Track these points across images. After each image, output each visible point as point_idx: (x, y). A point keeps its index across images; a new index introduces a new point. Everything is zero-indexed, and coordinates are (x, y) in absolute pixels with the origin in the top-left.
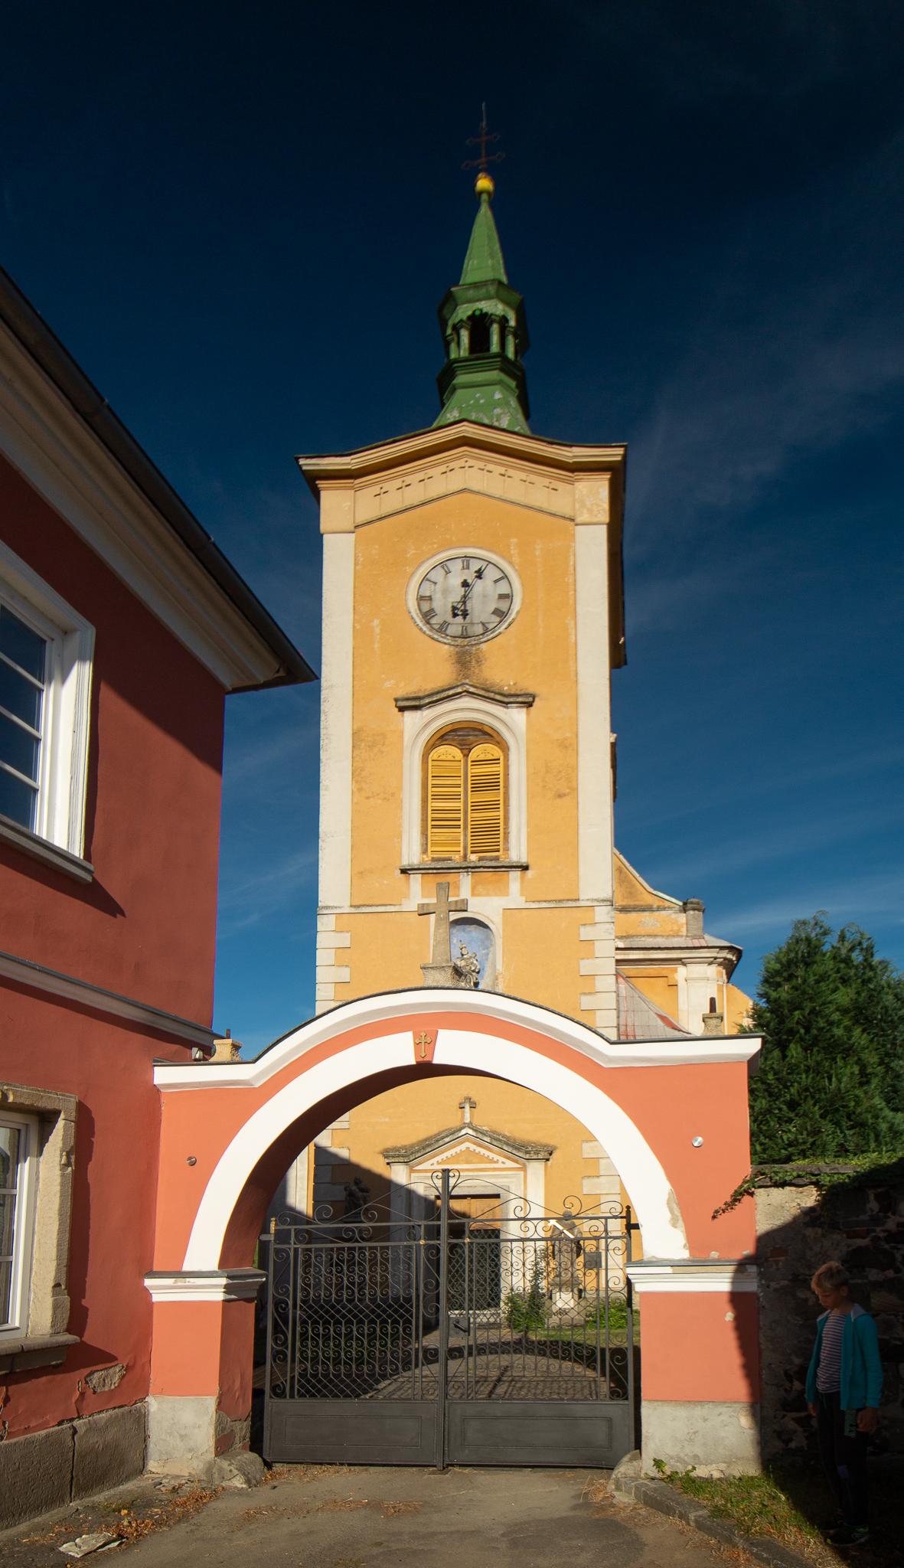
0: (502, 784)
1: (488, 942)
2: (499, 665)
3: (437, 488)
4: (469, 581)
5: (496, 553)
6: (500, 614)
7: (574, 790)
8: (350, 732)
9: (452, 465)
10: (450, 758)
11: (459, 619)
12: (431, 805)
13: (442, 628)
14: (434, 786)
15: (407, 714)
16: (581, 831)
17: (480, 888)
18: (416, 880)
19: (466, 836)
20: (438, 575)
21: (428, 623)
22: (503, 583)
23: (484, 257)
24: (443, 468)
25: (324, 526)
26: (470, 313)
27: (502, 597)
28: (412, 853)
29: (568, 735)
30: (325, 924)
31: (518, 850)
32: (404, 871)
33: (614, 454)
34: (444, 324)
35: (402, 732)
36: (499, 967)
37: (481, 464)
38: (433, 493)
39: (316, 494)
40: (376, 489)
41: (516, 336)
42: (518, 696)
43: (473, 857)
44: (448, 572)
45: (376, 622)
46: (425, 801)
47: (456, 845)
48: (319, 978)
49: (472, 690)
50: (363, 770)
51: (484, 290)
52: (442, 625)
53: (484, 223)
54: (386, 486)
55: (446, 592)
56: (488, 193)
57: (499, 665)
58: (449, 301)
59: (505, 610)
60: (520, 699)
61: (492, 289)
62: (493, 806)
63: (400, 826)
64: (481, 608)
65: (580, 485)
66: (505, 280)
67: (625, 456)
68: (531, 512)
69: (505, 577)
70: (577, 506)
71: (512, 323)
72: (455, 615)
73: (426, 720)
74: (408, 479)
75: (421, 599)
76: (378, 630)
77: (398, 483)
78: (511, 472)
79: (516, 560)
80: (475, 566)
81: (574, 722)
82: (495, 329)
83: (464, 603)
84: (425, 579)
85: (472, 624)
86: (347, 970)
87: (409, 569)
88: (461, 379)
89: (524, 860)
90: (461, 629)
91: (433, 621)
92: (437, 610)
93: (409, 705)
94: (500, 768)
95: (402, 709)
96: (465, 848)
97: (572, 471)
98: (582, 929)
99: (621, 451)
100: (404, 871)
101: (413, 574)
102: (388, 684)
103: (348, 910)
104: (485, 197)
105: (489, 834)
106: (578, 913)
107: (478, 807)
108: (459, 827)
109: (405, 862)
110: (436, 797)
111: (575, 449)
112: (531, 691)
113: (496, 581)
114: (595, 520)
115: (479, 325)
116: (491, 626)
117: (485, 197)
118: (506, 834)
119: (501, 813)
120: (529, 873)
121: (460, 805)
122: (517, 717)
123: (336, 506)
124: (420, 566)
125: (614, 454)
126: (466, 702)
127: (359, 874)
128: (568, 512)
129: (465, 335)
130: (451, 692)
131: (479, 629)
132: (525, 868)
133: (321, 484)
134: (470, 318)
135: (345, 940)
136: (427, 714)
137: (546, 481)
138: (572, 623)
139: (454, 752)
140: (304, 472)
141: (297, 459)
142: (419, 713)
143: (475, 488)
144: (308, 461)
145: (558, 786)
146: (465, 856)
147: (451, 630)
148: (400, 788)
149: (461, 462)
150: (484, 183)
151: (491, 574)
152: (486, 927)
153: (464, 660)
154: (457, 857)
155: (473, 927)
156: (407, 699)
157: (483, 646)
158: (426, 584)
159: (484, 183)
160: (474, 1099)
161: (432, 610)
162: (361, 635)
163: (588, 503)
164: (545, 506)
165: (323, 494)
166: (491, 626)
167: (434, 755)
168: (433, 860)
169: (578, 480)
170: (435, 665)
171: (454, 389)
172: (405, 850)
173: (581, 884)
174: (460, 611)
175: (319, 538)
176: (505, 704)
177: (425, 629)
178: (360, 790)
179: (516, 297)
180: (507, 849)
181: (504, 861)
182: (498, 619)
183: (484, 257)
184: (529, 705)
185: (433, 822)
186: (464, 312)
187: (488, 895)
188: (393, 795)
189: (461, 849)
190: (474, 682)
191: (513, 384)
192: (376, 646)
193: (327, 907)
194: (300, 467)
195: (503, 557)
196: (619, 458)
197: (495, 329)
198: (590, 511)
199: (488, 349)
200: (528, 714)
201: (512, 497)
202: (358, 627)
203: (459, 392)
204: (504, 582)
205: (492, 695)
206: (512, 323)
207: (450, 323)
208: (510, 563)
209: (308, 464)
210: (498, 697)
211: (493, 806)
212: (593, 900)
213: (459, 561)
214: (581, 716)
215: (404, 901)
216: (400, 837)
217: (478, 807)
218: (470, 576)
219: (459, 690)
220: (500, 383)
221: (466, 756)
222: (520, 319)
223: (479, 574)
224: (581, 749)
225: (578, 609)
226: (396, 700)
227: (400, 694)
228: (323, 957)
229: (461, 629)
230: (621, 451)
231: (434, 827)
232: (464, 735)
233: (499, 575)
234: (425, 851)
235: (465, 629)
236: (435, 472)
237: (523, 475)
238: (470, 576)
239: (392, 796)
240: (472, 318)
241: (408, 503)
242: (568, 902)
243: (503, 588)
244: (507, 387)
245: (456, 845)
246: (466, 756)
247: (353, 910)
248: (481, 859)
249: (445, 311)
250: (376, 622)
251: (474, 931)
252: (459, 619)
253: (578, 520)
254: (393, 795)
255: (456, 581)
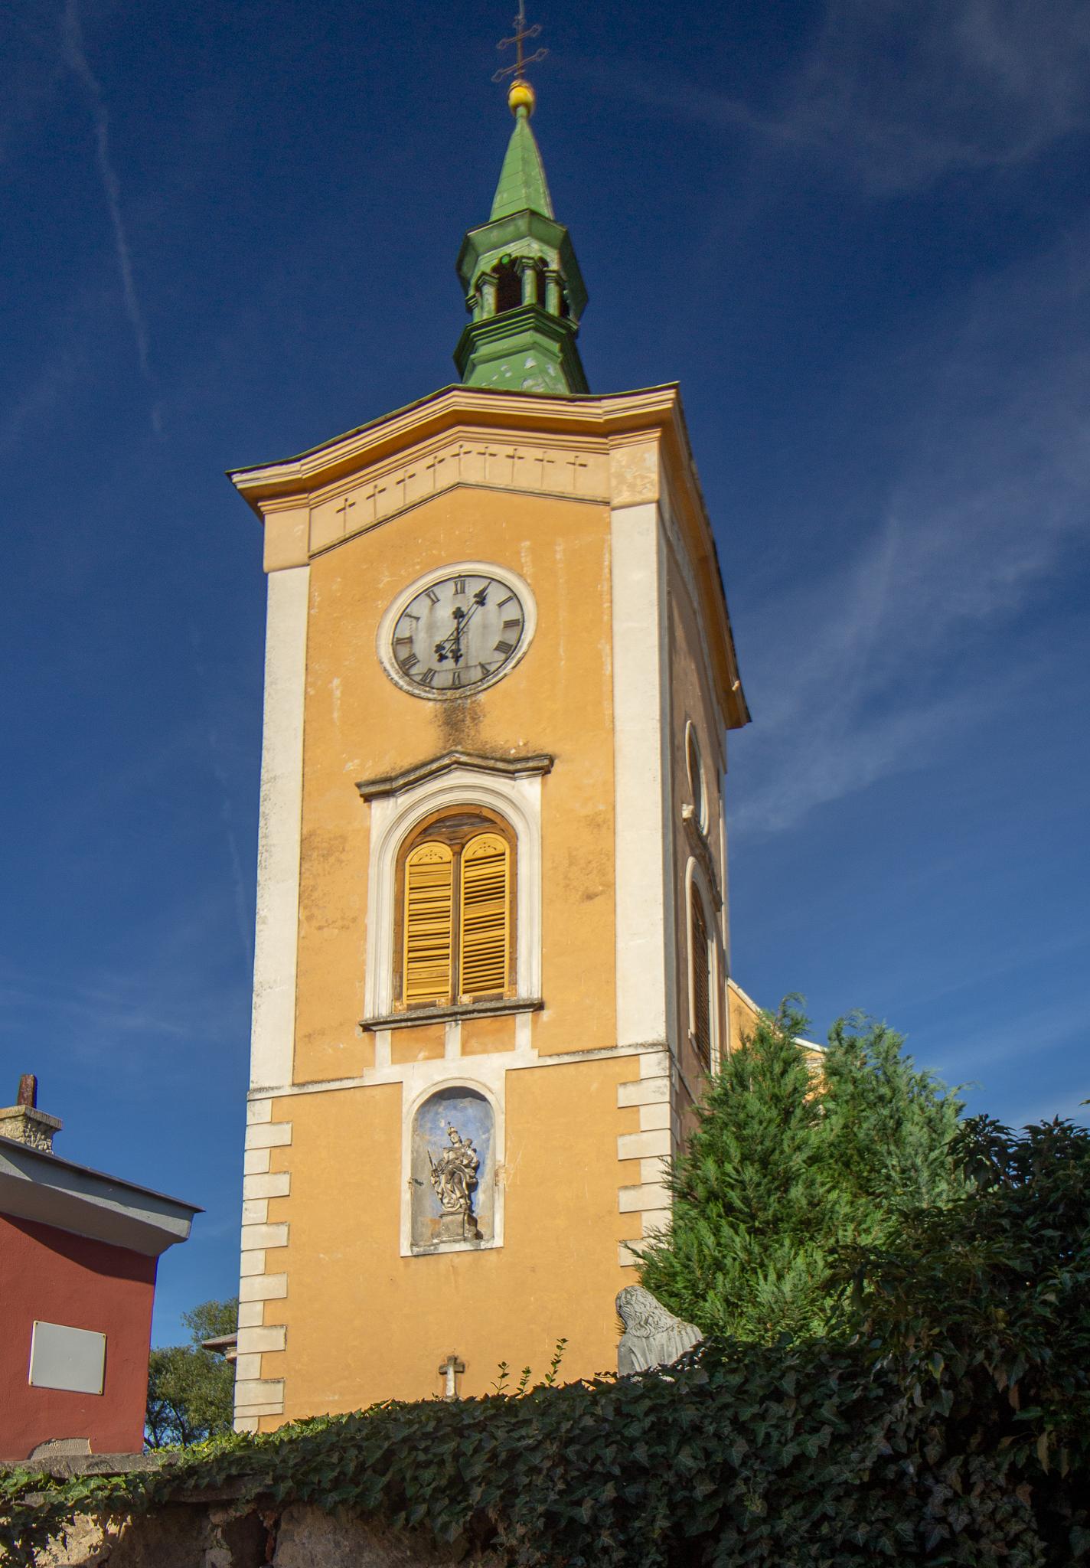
0: (507, 889)
1: (486, 1123)
2: (503, 722)
3: (419, 489)
4: (464, 609)
5: (500, 565)
6: (506, 648)
7: (610, 886)
8: (298, 837)
9: (441, 455)
10: (436, 859)
11: (449, 664)
12: (408, 928)
13: (426, 680)
14: (412, 902)
15: (375, 804)
16: (620, 945)
17: (474, 1043)
18: (384, 1040)
19: (456, 969)
20: (422, 608)
21: (407, 674)
22: (512, 606)
23: (522, 181)
24: (429, 460)
25: (267, 565)
26: (495, 262)
27: (509, 624)
28: (379, 1000)
29: (602, 807)
30: (258, 1113)
31: (528, 984)
32: (367, 1028)
33: (663, 400)
34: (465, 283)
35: (368, 831)
36: (500, 1157)
37: (481, 447)
38: (414, 497)
39: (261, 517)
40: (339, 503)
41: (560, 283)
42: (527, 759)
43: (465, 999)
44: (435, 601)
45: (336, 682)
46: (398, 924)
47: (436, 985)
48: (247, 1193)
49: (463, 759)
50: (314, 889)
51: (511, 229)
52: (425, 675)
53: (522, 141)
54: (352, 497)
55: (431, 627)
56: (526, 105)
57: (503, 722)
58: (467, 249)
59: (513, 642)
60: (531, 764)
61: (522, 224)
62: (496, 921)
63: (364, 963)
64: (479, 645)
65: (617, 454)
66: (547, 212)
67: (678, 401)
68: (548, 502)
69: (514, 597)
70: (614, 482)
71: (554, 266)
72: (442, 658)
73: (401, 810)
74: (381, 483)
75: (397, 642)
76: (338, 694)
77: (369, 489)
78: (522, 451)
79: (528, 570)
80: (474, 588)
81: (609, 789)
82: (529, 277)
83: (457, 640)
84: (405, 614)
85: (467, 667)
86: (286, 1178)
87: (380, 604)
88: (484, 350)
89: (536, 995)
90: (450, 674)
91: (413, 671)
92: (419, 656)
93: (378, 790)
94: (506, 867)
95: (368, 798)
96: (455, 986)
97: (606, 436)
98: (621, 1091)
99: (671, 394)
100: (367, 1028)
101: (386, 610)
102: (350, 766)
103: (288, 1091)
104: (522, 111)
105: (490, 963)
106: (615, 1067)
107: (473, 926)
108: (446, 957)
109: (368, 1015)
110: (415, 918)
111: (605, 403)
112: (549, 750)
113: (500, 605)
114: (638, 498)
115: (508, 277)
116: (492, 668)
117: (522, 111)
118: (514, 960)
119: (506, 931)
120: (545, 1015)
121: (448, 925)
122: (529, 790)
123: (284, 531)
124: (396, 598)
125: (663, 400)
126: (458, 778)
127: (305, 1038)
128: (600, 493)
129: (490, 294)
130: (435, 766)
131: (477, 674)
132: (538, 1007)
133: (265, 506)
134: (495, 269)
135: (282, 1135)
136: (404, 800)
137: (570, 456)
138: (608, 647)
139: (444, 851)
140: (241, 491)
141: (230, 475)
142: (392, 800)
143: (472, 480)
144: (245, 476)
145: (587, 883)
146: (454, 1000)
147: (437, 681)
148: (364, 909)
149: (455, 449)
150: (520, 93)
151: (495, 595)
152: (483, 1098)
153: (454, 720)
154: (443, 1002)
155: (466, 1102)
156: (373, 783)
157: (482, 697)
158: (406, 621)
159: (520, 93)
160: (462, 1358)
161: (413, 656)
162: (315, 702)
163: (629, 477)
164: (569, 490)
165: (268, 518)
166: (492, 668)
167: (413, 858)
168: (410, 1008)
169: (614, 447)
170: (413, 728)
171: (474, 366)
172: (368, 997)
173: (620, 1024)
174: (452, 651)
175: (264, 578)
176: (511, 774)
177: (401, 683)
178: (309, 918)
179: (559, 231)
180: (514, 982)
181: (509, 999)
182: (503, 656)
183: (522, 181)
184: (545, 771)
185: (406, 954)
186: (487, 262)
187: (485, 1051)
188: (354, 920)
189: (449, 988)
190: (470, 749)
191: (555, 347)
192: (336, 715)
193: (261, 1090)
194: (234, 485)
195: (510, 569)
196: (669, 405)
197: (529, 277)
198: (632, 487)
199: (519, 302)
200: (544, 784)
201: (523, 483)
202: (312, 692)
203: (480, 369)
204: (513, 604)
205: (491, 763)
206: (554, 266)
207: (473, 281)
208: (521, 576)
209: (243, 480)
210: (500, 765)
211: (496, 921)
212: (637, 1045)
213: (451, 584)
214: (618, 777)
215: (366, 1072)
216: (363, 979)
217: (473, 926)
218: (467, 602)
219: (446, 761)
220: (534, 346)
221: (458, 854)
222: (564, 261)
223: (481, 599)
224: (619, 826)
225: (616, 627)
226: (359, 786)
227: (367, 775)
228: (254, 1161)
229: (450, 674)
230: (671, 394)
231: (411, 960)
232: (454, 825)
233: (504, 595)
234: (398, 996)
235: (457, 676)
236: (418, 467)
237: (538, 453)
238: (467, 602)
239: (354, 923)
240: (498, 269)
241: (382, 514)
242: (601, 1053)
243: (511, 612)
244: (547, 352)
245: (436, 985)
246: (458, 854)
247: (296, 1091)
248: (476, 1000)
249: (465, 268)
250: (336, 682)
251: (469, 1107)
252: (449, 664)
253: (615, 502)
254: (354, 920)
255: (445, 612)
